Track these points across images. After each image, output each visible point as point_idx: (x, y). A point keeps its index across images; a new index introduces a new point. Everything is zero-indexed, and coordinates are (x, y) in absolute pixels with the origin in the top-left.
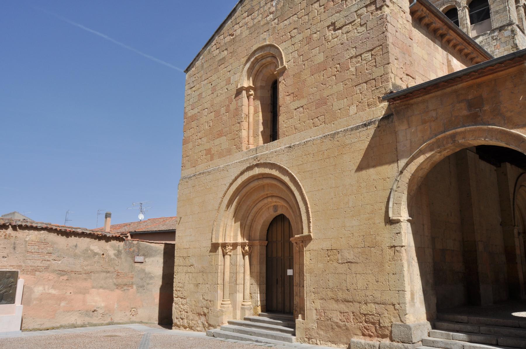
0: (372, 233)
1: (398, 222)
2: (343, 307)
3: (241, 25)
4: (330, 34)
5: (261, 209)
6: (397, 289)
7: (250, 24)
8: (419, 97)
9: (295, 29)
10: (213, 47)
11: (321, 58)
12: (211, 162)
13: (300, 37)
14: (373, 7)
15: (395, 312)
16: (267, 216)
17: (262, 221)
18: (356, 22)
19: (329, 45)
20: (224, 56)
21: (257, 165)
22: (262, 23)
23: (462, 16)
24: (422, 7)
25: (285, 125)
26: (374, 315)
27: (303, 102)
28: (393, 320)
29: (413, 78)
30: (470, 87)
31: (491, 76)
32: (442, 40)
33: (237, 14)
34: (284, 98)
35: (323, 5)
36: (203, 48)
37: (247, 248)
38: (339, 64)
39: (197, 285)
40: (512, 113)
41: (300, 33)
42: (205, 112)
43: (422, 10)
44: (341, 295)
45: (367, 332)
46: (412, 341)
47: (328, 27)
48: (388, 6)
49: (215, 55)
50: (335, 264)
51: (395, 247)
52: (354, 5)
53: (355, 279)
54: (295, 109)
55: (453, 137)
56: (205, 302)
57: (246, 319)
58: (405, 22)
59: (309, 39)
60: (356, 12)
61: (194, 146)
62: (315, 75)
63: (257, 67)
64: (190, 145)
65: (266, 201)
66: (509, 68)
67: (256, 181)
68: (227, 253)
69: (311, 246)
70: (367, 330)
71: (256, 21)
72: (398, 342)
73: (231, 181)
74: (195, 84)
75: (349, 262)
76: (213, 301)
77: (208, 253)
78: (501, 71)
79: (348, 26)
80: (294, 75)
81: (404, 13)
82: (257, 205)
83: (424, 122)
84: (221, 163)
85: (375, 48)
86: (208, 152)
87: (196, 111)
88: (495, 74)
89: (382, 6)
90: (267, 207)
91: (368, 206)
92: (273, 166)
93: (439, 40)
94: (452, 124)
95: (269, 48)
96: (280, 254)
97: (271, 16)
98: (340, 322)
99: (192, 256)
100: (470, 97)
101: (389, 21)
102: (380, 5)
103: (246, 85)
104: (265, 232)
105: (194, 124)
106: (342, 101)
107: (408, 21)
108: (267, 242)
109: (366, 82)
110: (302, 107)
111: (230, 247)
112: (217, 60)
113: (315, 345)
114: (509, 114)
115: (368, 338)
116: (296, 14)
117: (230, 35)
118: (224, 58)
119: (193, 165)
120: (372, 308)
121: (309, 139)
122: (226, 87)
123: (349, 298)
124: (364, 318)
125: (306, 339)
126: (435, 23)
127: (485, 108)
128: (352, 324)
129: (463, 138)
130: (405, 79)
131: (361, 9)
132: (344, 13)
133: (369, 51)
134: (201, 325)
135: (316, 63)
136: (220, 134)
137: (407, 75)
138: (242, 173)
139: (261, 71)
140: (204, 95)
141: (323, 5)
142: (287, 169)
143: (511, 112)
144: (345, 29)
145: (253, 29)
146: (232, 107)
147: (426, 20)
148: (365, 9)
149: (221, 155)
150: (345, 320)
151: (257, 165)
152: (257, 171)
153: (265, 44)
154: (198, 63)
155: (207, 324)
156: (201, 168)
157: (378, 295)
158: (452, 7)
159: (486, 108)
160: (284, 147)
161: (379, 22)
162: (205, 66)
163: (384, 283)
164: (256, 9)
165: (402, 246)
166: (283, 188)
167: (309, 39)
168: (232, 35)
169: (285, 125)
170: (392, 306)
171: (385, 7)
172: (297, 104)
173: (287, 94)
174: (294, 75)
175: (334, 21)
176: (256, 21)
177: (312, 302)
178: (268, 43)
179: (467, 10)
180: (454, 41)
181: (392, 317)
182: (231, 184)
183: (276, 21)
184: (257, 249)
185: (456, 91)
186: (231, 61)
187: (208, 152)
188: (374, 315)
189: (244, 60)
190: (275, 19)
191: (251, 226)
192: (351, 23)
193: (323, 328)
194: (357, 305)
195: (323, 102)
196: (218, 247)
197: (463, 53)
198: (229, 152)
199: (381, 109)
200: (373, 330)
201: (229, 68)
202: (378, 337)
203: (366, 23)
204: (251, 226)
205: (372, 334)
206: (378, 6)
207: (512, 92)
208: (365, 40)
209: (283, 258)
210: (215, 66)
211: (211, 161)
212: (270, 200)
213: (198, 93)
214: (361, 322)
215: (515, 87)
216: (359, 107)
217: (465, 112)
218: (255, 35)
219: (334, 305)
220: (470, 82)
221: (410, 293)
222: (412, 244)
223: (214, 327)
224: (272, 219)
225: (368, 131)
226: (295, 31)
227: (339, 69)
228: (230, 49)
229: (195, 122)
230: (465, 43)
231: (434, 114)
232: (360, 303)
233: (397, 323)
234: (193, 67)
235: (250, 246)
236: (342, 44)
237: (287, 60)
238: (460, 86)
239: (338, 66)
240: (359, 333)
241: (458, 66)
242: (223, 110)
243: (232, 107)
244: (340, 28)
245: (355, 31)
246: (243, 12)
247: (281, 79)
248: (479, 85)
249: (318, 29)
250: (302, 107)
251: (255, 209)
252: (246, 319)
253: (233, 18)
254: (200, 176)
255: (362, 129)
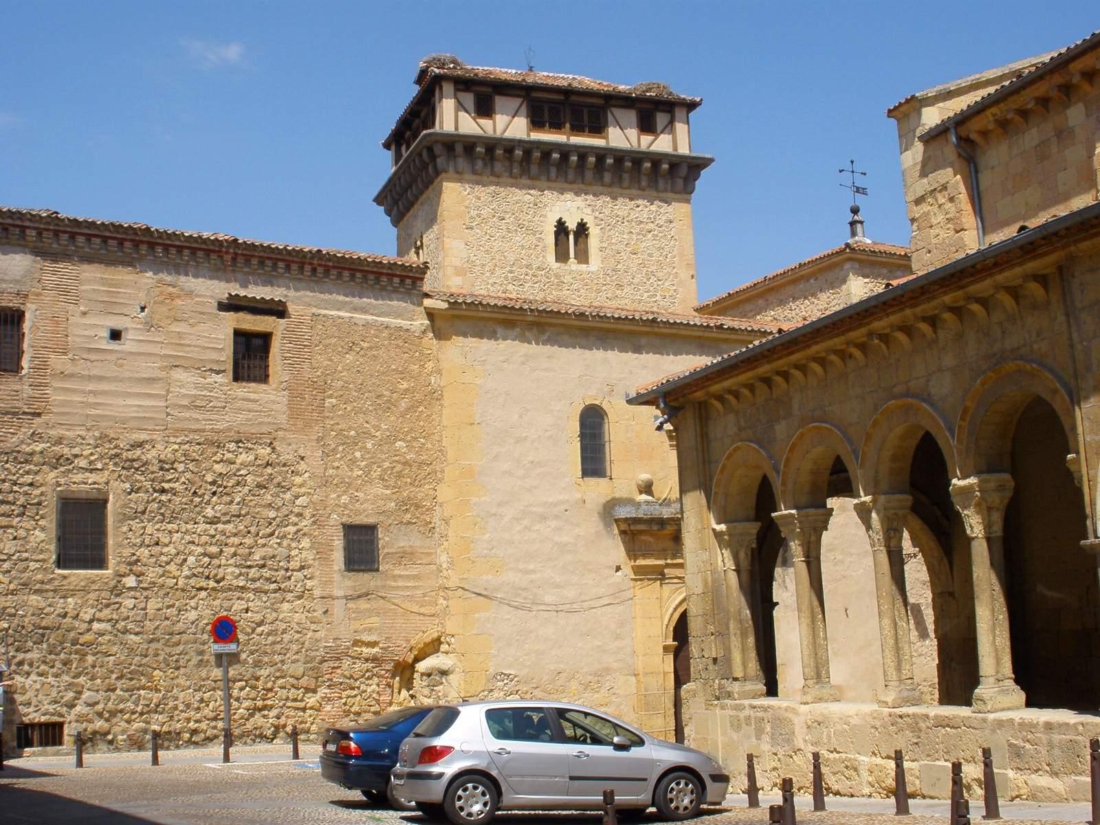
43: (994, 115)
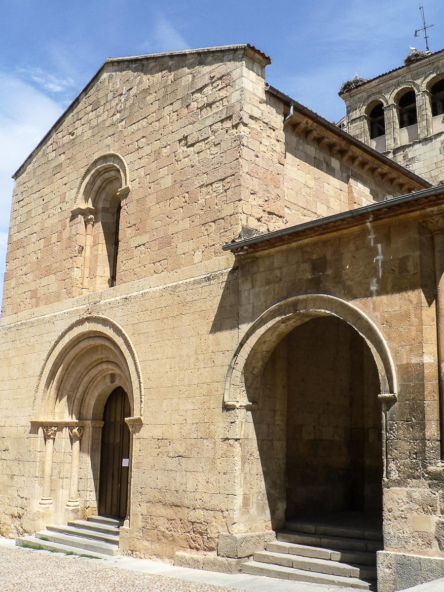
0: (206, 421)
1: (233, 409)
2: (170, 512)
3: (83, 123)
4: (182, 149)
5: (95, 377)
6: (227, 492)
7: (94, 123)
8: (264, 250)
9: (143, 137)
10: (48, 148)
11: (168, 182)
12: (36, 309)
13: (147, 150)
14: (228, 124)
15: (223, 520)
16: (103, 388)
17: (97, 394)
18: (209, 140)
19: (179, 166)
20: (61, 162)
21: (88, 319)
22: (107, 124)
23: (421, 104)
24: (306, 119)
25: (123, 268)
26: (202, 523)
27: (144, 239)
28: (221, 529)
29: (280, 217)
30: (315, 244)
31: (335, 234)
32: (342, 158)
33: (80, 106)
34: (124, 231)
35: (176, 111)
36: (37, 148)
37: (75, 430)
38: (188, 192)
39: (12, 477)
40: (352, 282)
41: (148, 144)
42: (34, 238)
44: (169, 498)
45: (193, 544)
46: (236, 556)
47: (180, 141)
48: (245, 125)
49: (50, 159)
50: (165, 458)
51: (228, 439)
52: (209, 117)
53: (185, 477)
54: (136, 247)
55: (295, 305)
56: (20, 501)
57: (70, 524)
58: (275, 142)
59: (158, 153)
60: (211, 126)
61: (18, 285)
62: (162, 204)
63: (98, 183)
64: (13, 282)
65: (100, 368)
66: (351, 227)
67: (86, 340)
68: (49, 436)
69: (144, 432)
70: (194, 541)
71: (101, 119)
72: (223, 556)
73: (56, 338)
74: (24, 196)
75: (180, 456)
76: (29, 499)
77: (27, 434)
78: (345, 228)
79: (200, 144)
80: (138, 201)
81: (274, 130)
82: (90, 373)
83: (268, 282)
84: (47, 312)
85: (226, 178)
86: (34, 293)
87: (22, 235)
88: (339, 232)
89: (238, 124)
90: (103, 375)
91: (205, 385)
92: (105, 322)
93: (337, 158)
94: (295, 289)
95: (113, 158)
96: (118, 440)
97: (118, 115)
98: (167, 532)
99: (8, 436)
100: (314, 257)
101: (245, 144)
102: (236, 122)
103: (83, 206)
104: (101, 409)
105: (19, 253)
106: (186, 243)
107: (278, 141)
108: (102, 424)
109: (214, 222)
110: (144, 245)
111: (53, 428)
112: (52, 166)
113: (139, 559)
114: (349, 283)
115: (194, 551)
116: (146, 118)
117: (70, 134)
118: (60, 165)
119: (15, 311)
120: (199, 515)
121: (148, 290)
122: (60, 206)
123: (177, 502)
124: (191, 527)
125: (129, 552)
126: (327, 138)
127: (327, 273)
128: (179, 534)
129: (305, 308)
130: (266, 218)
131: (216, 123)
132: (198, 126)
133: (220, 180)
134: (15, 531)
135: (163, 187)
136: (48, 272)
137: (270, 213)
138: (71, 328)
139: (104, 187)
140: (33, 214)
141: (176, 111)
142: (121, 328)
143: (351, 281)
144: (197, 148)
145: (96, 130)
146: (66, 234)
147: (315, 134)
148: (220, 124)
149: (48, 301)
150: (172, 529)
151: (88, 319)
152: (87, 327)
153: (108, 152)
154: (30, 168)
155: (21, 530)
156: (24, 316)
157: (206, 498)
158: (408, 91)
159: (329, 272)
160: (119, 297)
161: (234, 145)
162: (38, 173)
163: (215, 484)
164: (102, 103)
165: (236, 440)
166: (117, 352)
167: (158, 153)
168: (73, 135)
169: (123, 268)
170: (220, 513)
171: (241, 125)
172: (139, 240)
173: (129, 225)
174: (138, 201)
175: (186, 135)
176: (101, 119)
177: (137, 505)
178: (112, 152)
179: (395, 110)
180: (360, 159)
181: (219, 526)
182: (57, 342)
183: (123, 123)
184: (89, 431)
185: (301, 248)
186: (68, 170)
187: (34, 293)
188: (202, 523)
189: (83, 171)
190: (122, 120)
191: (82, 401)
192: (204, 140)
193: (149, 539)
194: (186, 511)
195: (166, 242)
196: (381, 404)
197: (376, 173)
198: (57, 297)
199: (228, 261)
200: (201, 542)
201: (65, 180)
202: (205, 550)
203: (219, 143)
204: (82, 401)
205: (198, 546)
206: (234, 124)
207: (354, 257)
208: (217, 166)
209: (121, 444)
210: (49, 175)
211: (36, 307)
212: (104, 366)
213: (26, 209)
214: (189, 532)
215: (357, 250)
216: (205, 253)
217: (309, 276)
218: (97, 138)
219: (160, 510)
220: (316, 238)
221: (242, 497)
222: (253, 435)
223: (29, 533)
224: (111, 392)
225: (211, 287)
226: (144, 140)
227: (187, 199)
228: (69, 154)
229: (21, 250)
230: (377, 162)
231: (278, 273)
232: (188, 508)
233: (224, 534)
234: (23, 172)
235: (82, 428)
236: (192, 167)
237: (130, 180)
238: (306, 241)
239: (187, 195)
240: (185, 544)
241: (362, 196)
242: (54, 238)
243: (66, 234)
244: (192, 145)
245: (208, 151)
246: (87, 105)
247: (123, 202)
248: (325, 243)
249: (169, 143)
250: (144, 245)
251: (87, 379)
252: (70, 524)
253: (75, 111)
254: (22, 327)
255: (205, 284)
